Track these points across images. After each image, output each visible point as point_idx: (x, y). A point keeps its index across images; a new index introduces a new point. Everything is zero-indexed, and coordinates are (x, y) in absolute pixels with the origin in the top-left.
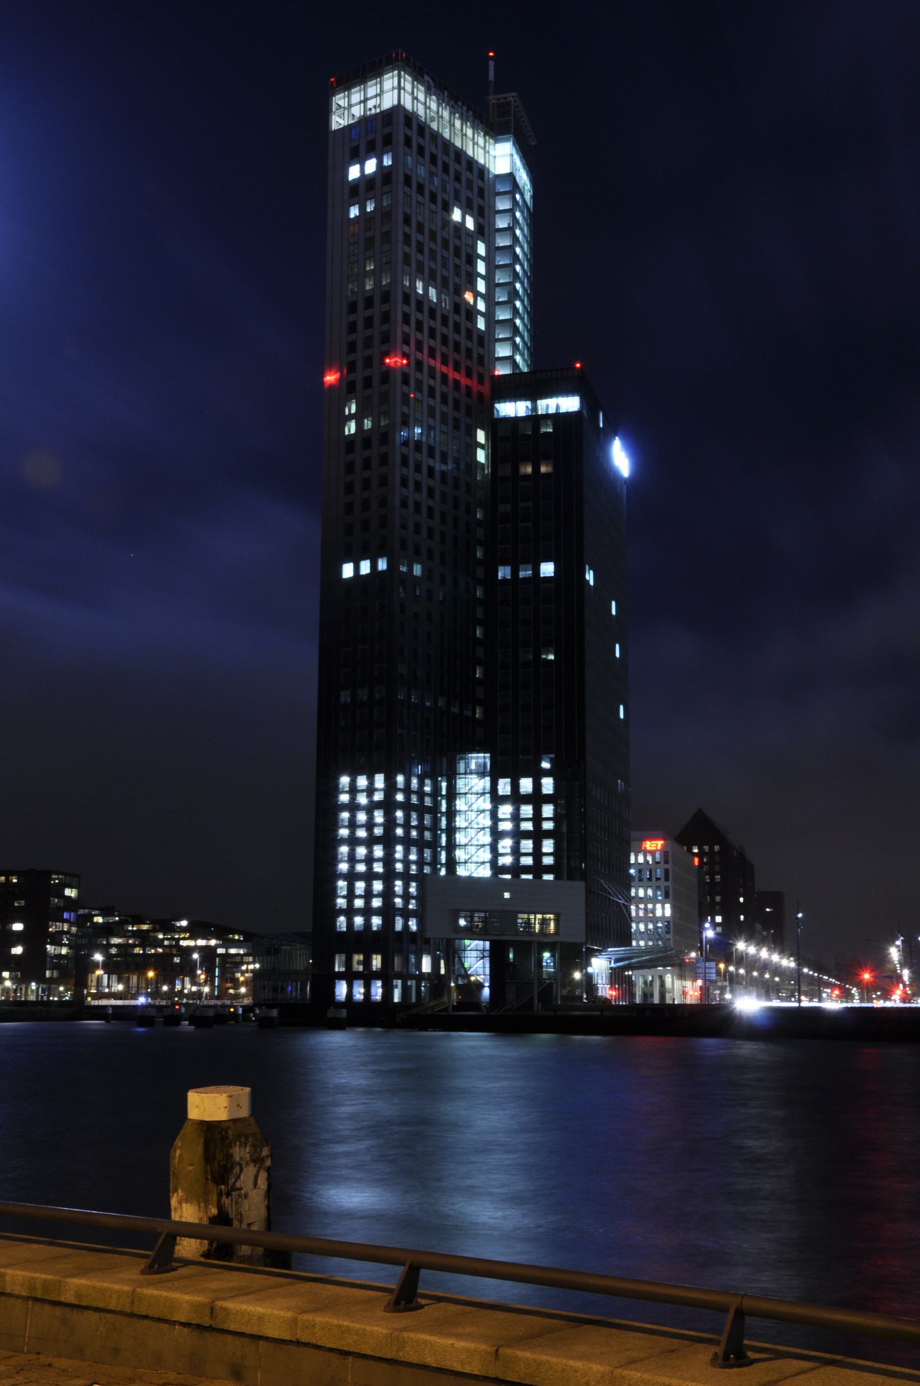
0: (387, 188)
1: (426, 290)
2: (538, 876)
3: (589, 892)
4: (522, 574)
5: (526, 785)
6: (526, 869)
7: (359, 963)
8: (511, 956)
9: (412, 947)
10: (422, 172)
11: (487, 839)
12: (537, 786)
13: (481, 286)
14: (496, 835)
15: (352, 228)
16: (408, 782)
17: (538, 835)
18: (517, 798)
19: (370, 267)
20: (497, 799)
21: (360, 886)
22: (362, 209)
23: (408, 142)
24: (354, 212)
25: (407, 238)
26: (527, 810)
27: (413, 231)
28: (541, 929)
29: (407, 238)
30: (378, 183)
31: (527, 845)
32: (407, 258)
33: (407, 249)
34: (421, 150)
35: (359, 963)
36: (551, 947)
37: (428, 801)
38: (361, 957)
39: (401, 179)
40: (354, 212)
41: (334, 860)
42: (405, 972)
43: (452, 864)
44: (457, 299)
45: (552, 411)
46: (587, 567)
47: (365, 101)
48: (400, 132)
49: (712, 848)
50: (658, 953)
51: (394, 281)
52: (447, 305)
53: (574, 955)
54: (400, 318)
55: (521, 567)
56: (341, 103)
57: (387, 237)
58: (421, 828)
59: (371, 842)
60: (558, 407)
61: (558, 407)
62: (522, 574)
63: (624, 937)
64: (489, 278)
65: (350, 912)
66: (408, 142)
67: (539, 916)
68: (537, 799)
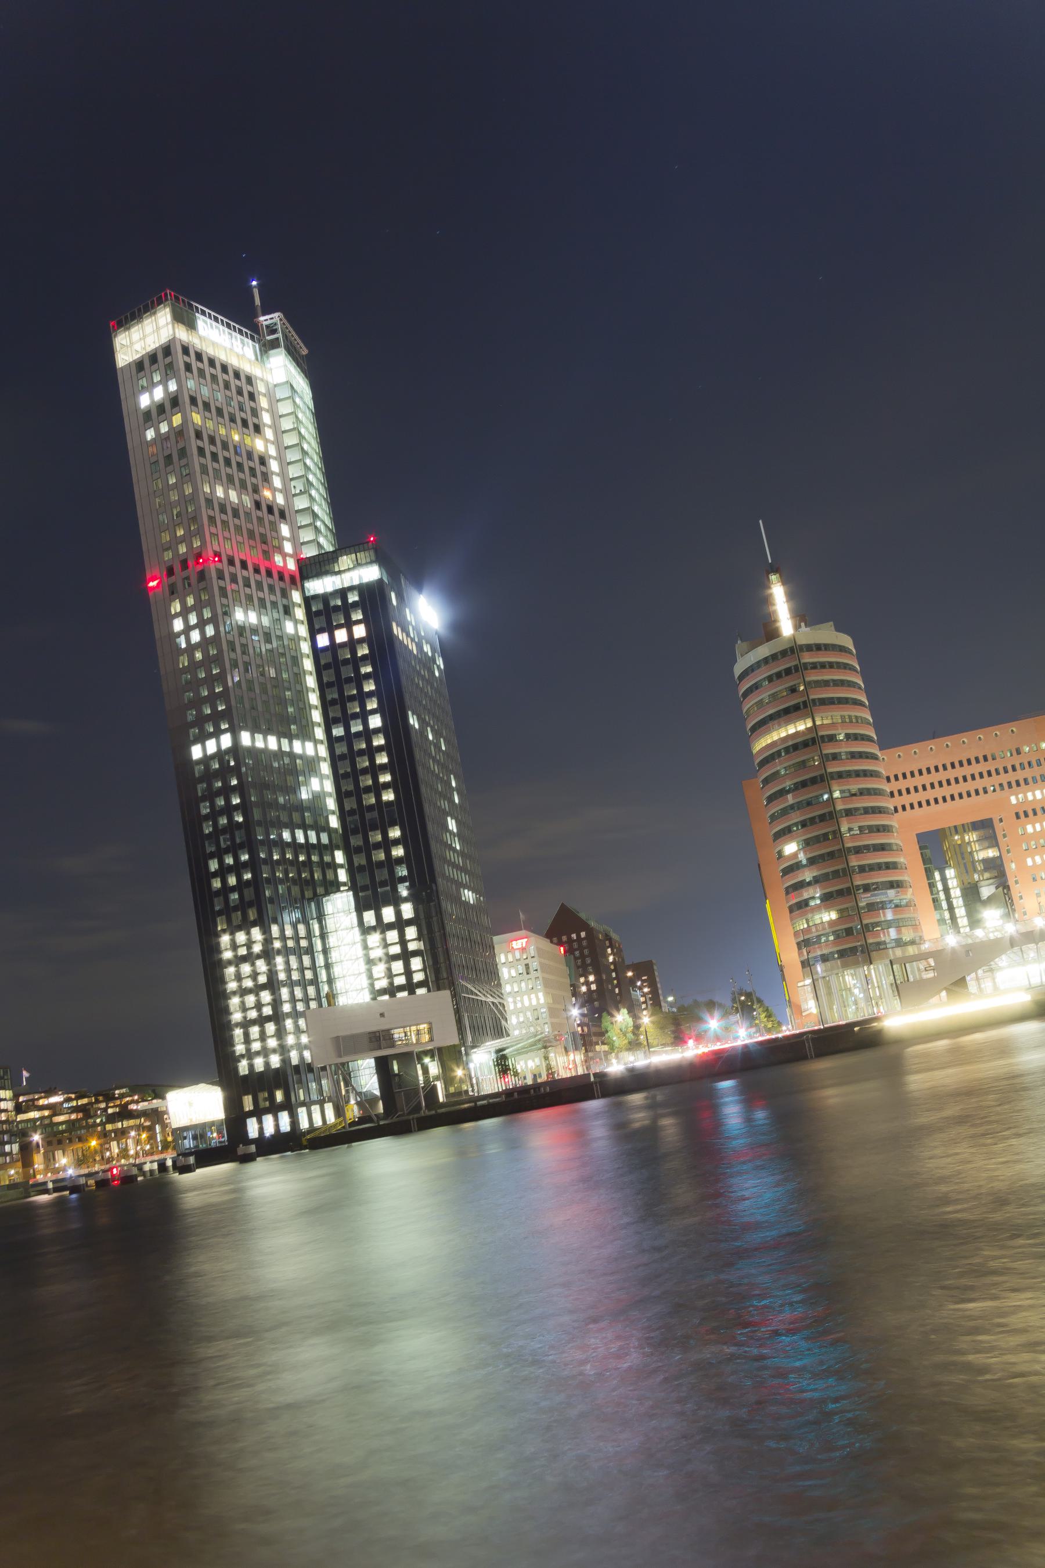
0: (202, 585)
1: (226, 493)
2: (412, 992)
3: (454, 996)
4: (354, 730)
5: (388, 914)
6: (401, 988)
7: (265, 1099)
8: (396, 1068)
9: (310, 1076)
10: (205, 391)
11: (362, 967)
12: (398, 913)
13: (277, 482)
14: (370, 962)
15: (150, 449)
16: (282, 931)
17: (406, 956)
18: (382, 927)
19: (172, 480)
20: (365, 930)
21: (255, 1031)
22: (157, 431)
23: (188, 367)
24: (150, 434)
25: (201, 451)
26: (393, 936)
27: (205, 444)
28: (418, 1040)
29: (201, 451)
30: (168, 406)
31: (398, 966)
32: (204, 470)
33: (203, 460)
34: (201, 373)
35: (265, 1099)
36: (430, 1053)
37: (304, 943)
38: (266, 1095)
39: (187, 400)
40: (150, 434)
41: (227, 1011)
42: (307, 1100)
43: (331, 997)
44: (257, 497)
45: (356, 582)
46: (410, 713)
47: (144, 337)
48: (180, 359)
49: (578, 936)
50: (528, 1039)
51: (196, 489)
52: (247, 501)
53: (450, 1056)
54: (214, 575)
55: (352, 723)
56: (124, 342)
57: (183, 453)
58: (302, 969)
59: (258, 989)
60: (360, 578)
61: (360, 578)
62: (354, 730)
63: (499, 1031)
64: (283, 474)
65: (250, 1055)
66: (188, 367)
67: (414, 1028)
68: (400, 924)
